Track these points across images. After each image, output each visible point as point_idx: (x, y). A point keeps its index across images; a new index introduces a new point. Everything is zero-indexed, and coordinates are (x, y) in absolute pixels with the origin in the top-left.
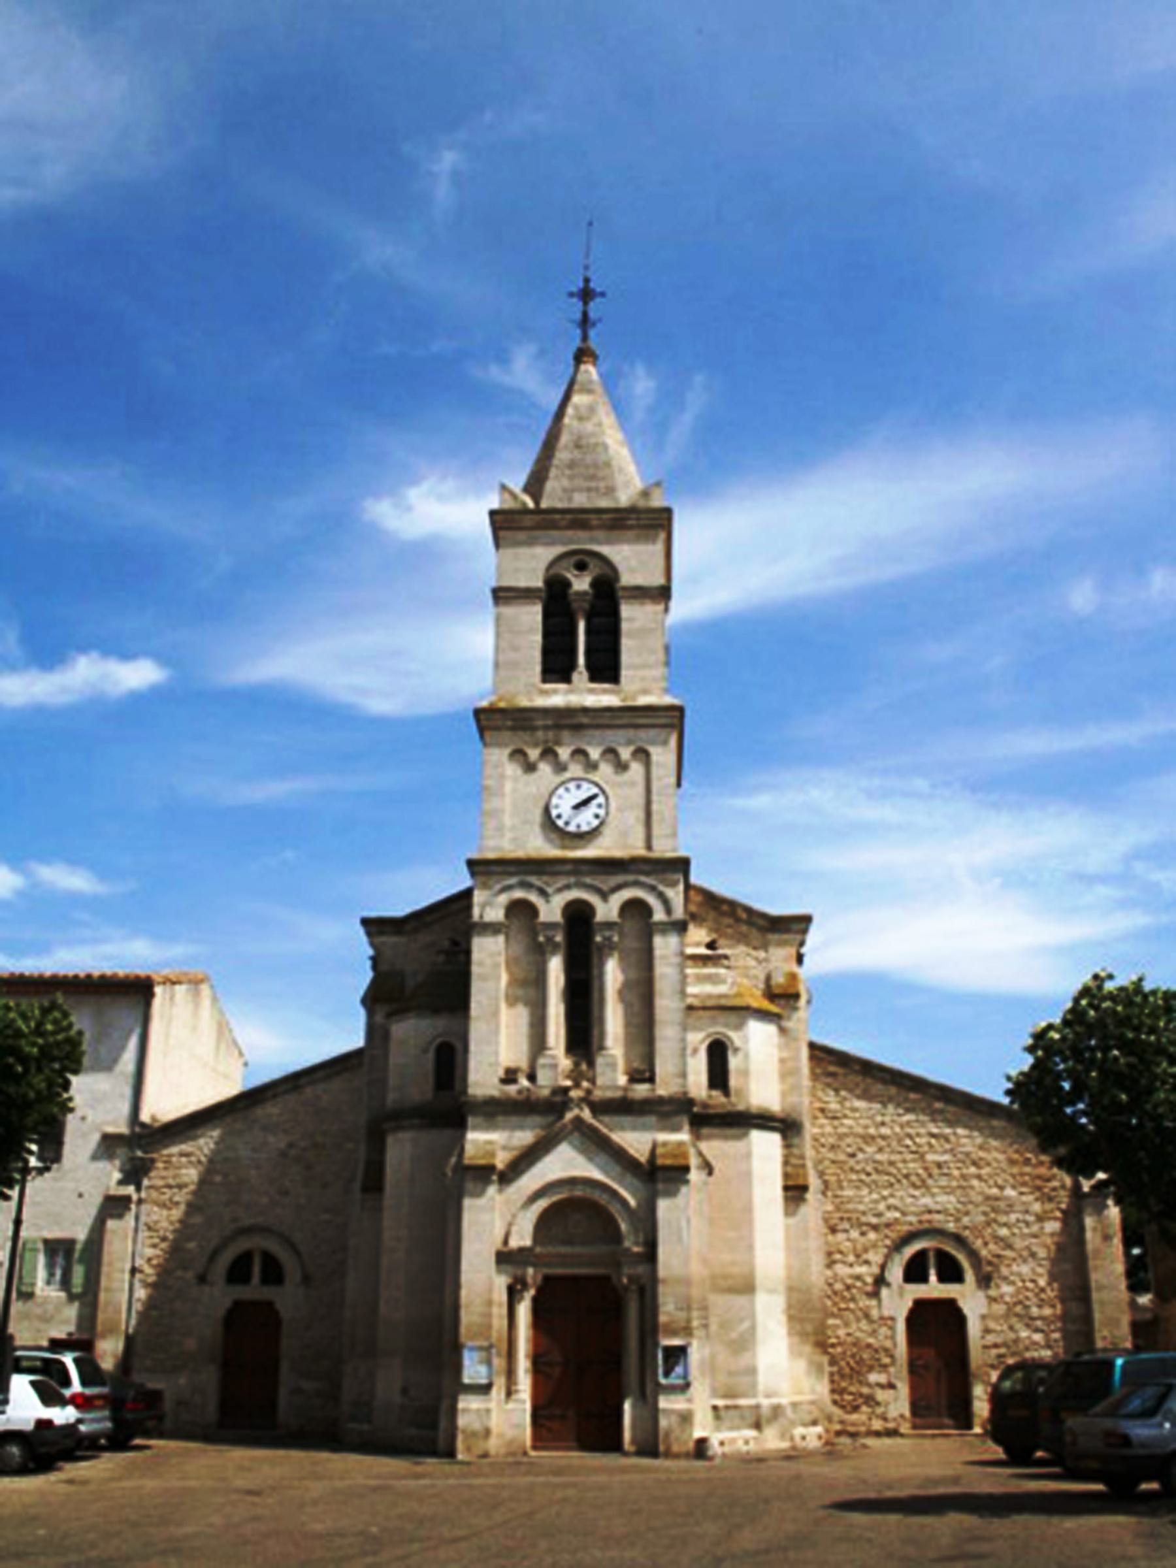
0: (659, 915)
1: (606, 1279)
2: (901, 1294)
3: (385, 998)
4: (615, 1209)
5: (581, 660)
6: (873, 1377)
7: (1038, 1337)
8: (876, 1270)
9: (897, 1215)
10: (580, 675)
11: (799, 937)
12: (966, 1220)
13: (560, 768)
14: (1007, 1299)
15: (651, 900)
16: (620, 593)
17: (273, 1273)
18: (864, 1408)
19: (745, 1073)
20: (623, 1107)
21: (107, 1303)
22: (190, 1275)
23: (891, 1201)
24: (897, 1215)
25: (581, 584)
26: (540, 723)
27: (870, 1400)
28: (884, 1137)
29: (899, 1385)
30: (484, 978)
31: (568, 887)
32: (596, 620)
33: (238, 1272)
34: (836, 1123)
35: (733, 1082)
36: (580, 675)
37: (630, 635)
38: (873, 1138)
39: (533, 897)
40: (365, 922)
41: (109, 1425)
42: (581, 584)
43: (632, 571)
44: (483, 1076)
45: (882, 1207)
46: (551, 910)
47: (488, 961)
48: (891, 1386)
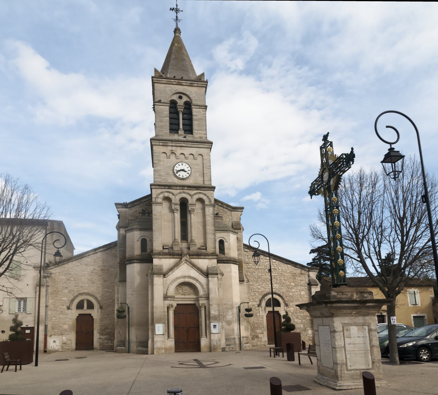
0: (207, 202)
1: (195, 304)
2: (265, 309)
3: (124, 225)
4: (197, 285)
5: (181, 126)
6: (258, 331)
7: (300, 321)
8: (258, 303)
9: (264, 289)
10: (181, 132)
11: (241, 213)
12: (281, 291)
13: (177, 158)
14: (292, 311)
15: (204, 198)
16: (193, 107)
17: (91, 306)
18: (255, 339)
19: (229, 249)
20: (198, 255)
21: (116, 256)
22: (65, 307)
23: (262, 286)
24: (264, 289)
25: (181, 103)
26: (170, 144)
27: (257, 337)
28: (260, 269)
29: (264, 332)
30: (157, 219)
31: (180, 193)
32: (185, 115)
33: (80, 306)
34: (247, 265)
35: (226, 251)
36: (181, 132)
37: (197, 120)
38: (257, 269)
39: (171, 196)
40: (116, 204)
41: (375, 274)
42: (181, 103)
43: (196, 100)
44: (157, 246)
45: (259, 287)
46: (176, 199)
47: (158, 214)
48: (263, 333)
